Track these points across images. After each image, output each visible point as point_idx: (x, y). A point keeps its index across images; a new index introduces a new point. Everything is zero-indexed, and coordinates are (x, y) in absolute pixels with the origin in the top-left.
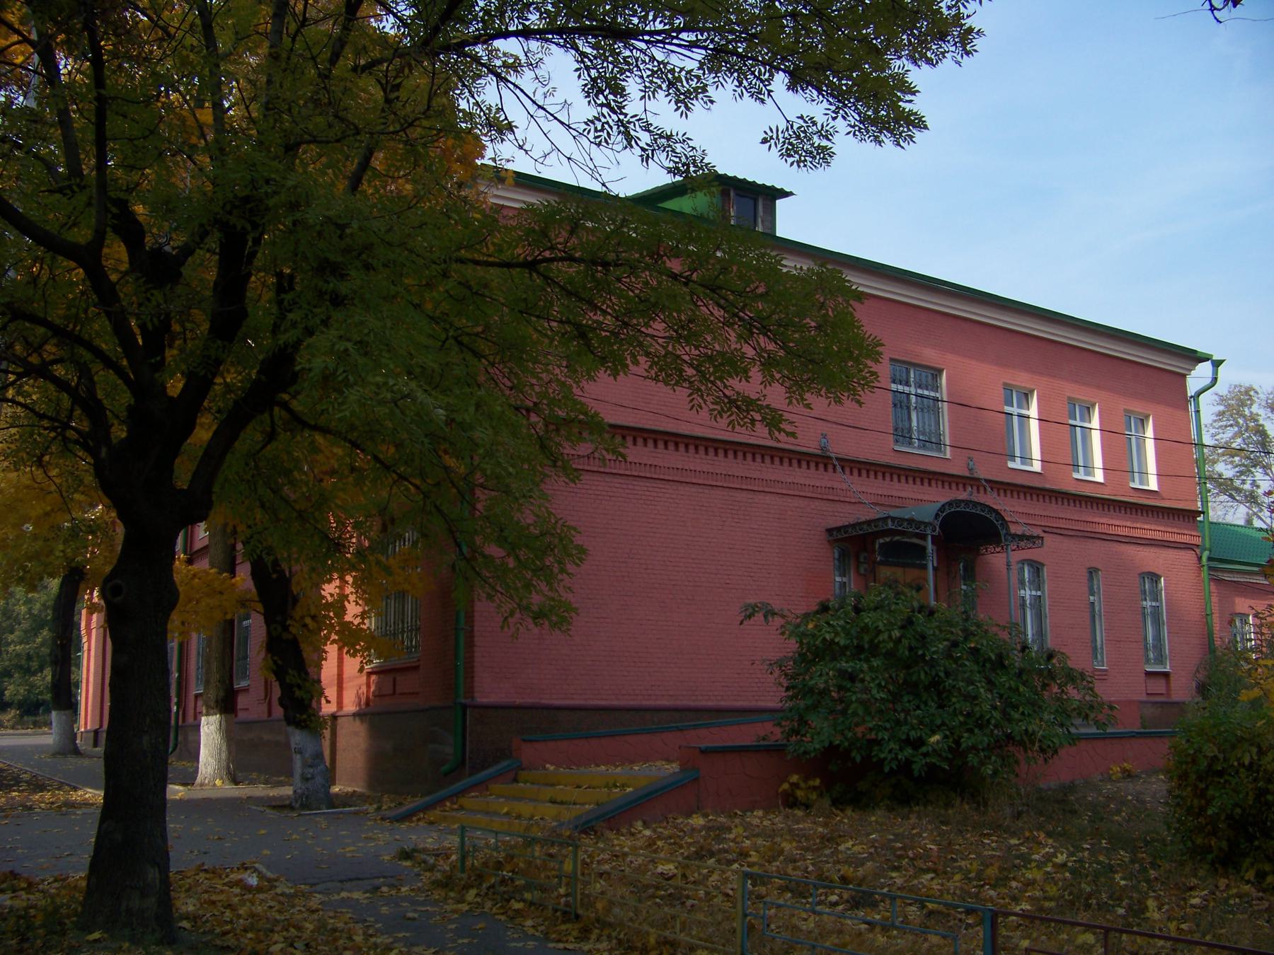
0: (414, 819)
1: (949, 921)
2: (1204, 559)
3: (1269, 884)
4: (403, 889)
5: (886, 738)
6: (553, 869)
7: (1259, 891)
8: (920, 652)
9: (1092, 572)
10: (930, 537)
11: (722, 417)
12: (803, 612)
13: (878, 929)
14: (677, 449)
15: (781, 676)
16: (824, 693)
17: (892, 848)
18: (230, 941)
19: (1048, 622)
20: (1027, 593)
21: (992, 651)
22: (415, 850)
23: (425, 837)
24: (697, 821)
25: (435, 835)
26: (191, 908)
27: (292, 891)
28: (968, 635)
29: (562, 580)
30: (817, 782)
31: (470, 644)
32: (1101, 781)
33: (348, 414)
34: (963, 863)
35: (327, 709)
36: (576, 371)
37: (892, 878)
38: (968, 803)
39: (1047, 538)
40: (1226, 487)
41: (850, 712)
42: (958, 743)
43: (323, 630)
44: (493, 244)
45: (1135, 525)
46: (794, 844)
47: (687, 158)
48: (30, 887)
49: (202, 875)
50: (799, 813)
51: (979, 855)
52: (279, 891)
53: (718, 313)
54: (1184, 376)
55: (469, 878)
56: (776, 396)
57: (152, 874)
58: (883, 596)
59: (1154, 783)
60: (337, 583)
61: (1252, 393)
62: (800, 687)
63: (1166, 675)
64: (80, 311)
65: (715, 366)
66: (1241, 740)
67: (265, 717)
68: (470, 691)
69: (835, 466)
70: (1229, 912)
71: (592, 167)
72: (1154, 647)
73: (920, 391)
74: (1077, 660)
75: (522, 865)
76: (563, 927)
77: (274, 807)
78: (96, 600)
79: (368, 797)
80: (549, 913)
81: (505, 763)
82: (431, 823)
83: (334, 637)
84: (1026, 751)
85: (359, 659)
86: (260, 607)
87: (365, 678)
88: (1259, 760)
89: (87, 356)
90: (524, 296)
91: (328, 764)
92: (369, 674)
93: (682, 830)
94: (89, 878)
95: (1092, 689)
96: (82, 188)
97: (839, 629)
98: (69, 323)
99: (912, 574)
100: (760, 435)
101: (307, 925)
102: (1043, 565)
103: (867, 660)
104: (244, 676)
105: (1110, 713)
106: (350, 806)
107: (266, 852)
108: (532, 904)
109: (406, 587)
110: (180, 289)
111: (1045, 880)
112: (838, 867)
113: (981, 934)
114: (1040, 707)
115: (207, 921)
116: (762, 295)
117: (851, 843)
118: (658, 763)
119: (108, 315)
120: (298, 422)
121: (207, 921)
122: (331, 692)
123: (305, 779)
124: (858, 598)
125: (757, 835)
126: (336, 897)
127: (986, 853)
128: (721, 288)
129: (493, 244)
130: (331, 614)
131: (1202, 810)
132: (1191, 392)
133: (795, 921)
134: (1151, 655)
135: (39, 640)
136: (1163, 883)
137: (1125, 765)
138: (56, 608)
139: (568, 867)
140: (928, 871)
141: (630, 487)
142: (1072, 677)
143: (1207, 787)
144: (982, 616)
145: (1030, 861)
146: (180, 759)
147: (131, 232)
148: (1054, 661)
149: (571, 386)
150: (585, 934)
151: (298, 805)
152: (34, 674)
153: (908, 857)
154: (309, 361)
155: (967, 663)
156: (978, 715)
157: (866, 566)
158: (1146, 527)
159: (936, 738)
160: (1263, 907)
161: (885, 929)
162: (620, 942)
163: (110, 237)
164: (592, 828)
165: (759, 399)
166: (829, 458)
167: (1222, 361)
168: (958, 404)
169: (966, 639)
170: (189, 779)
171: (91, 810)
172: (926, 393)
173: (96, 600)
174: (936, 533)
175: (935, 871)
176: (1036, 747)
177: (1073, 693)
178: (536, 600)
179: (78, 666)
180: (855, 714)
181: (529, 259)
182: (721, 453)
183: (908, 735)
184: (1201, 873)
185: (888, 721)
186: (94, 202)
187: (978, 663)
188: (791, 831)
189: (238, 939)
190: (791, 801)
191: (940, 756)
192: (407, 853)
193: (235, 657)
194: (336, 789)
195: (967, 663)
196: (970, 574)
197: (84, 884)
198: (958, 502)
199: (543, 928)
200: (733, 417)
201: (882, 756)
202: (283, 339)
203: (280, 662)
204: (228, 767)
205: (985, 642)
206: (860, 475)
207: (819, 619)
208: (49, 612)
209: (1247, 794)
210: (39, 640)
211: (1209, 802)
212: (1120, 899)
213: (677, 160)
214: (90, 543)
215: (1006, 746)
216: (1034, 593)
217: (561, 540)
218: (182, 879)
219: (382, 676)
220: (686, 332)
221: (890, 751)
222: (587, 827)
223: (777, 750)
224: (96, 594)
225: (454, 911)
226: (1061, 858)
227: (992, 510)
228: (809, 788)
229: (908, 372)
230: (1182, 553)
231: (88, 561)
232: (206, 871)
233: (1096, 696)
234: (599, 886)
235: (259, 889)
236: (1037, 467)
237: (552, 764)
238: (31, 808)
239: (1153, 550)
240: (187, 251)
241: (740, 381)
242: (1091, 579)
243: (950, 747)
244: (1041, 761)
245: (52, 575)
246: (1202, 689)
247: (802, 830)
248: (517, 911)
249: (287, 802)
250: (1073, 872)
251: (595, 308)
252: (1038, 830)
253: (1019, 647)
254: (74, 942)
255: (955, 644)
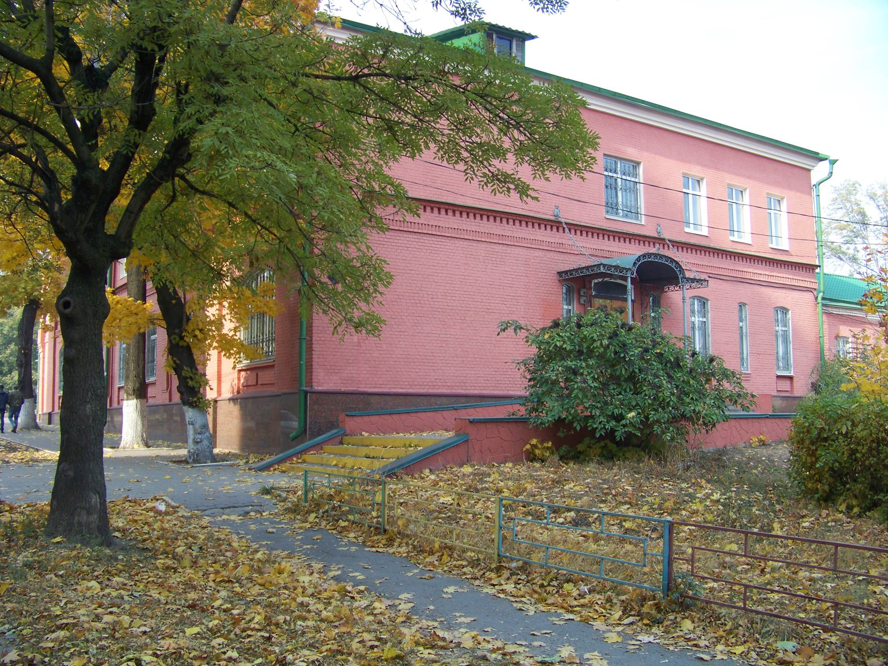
0: (272, 469)
1: (639, 536)
2: (819, 299)
3: (855, 513)
4: (264, 514)
5: (598, 414)
6: (368, 500)
7: (848, 518)
8: (622, 355)
9: (742, 305)
10: (629, 279)
11: (487, 186)
12: (542, 327)
13: (591, 540)
14: (454, 215)
15: (525, 371)
16: (555, 383)
17: (601, 488)
18: (149, 545)
19: (710, 340)
20: (697, 319)
21: (672, 355)
22: (272, 488)
23: (277, 480)
24: (467, 469)
25: (286, 479)
26: (121, 525)
27: (189, 514)
28: (655, 344)
29: (375, 297)
30: (550, 444)
31: (310, 349)
32: (744, 447)
33: (228, 176)
34: (649, 499)
35: (210, 395)
36: (385, 155)
37: (600, 508)
38: (653, 459)
39: (711, 281)
40: (838, 254)
41: (573, 396)
42: (647, 418)
43: (207, 340)
44: (328, 63)
45: (772, 274)
46: (534, 485)
47: (465, 4)
48: (12, 509)
49: (128, 504)
50: (537, 465)
51: (660, 493)
52: (180, 514)
53: (487, 114)
54: (809, 170)
55: (310, 506)
56: (525, 173)
57: (95, 499)
58: (597, 316)
59: (781, 449)
60: (217, 307)
61: (857, 185)
62: (539, 378)
63: (791, 378)
64: (38, 108)
65: (483, 151)
66: (841, 417)
67: (167, 402)
68: (310, 382)
69: (564, 229)
70: (828, 531)
71: (398, 11)
72: (783, 358)
73: (624, 177)
74: (730, 364)
75: (346, 497)
76: (376, 538)
77: (174, 462)
78: (48, 322)
79: (239, 455)
80: (366, 528)
81: (334, 431)
82: (284, 472)
83: (215, 344)
84: (693, 425)
85: (232, 360)
86: (164, 323)
87: (236, 375)
88: (852, 430)
89: (42, 140)
90: (350, 100)
91: (211, 432)
92: (240, 371)
93: (457, 476)
94: (51, 504)
95: (739, 383)
96: (36, 18)
97: (566, 339)
98: (30, 116)
99: (617, 304)
100: (511, 203)
101: (200, 536)
102: (708, 300)
103: (585, 360)
104: (153, 374)
105: (752, 399)
106: (227, 461)
107: (170, 490)
108: (354, 522)
109: (265, 309)
110: (107, 95)
111: (705, 511)
112: (564, 500)
113: (661, 544)
114: (704, 395)
115: (132, 532)
116: (516, 101)
117: (573, 484)
118: (440, 432)
119: (58, 109)
120: (192, 188)
121: (132, 532)
122: (213, 383)
123: (196, 442)
124: (580, 318)
125: (508, 479)
126: (219, 519)
127: (665, 492)
128: (487, 95)
129: (328, 63)
130: (214, 328)
131: (813, 464)
132: (814, 182)
133: (535, 534)
134: (781, 365)
135: (8, 352)
136: (784, 513)
137: (761, 437)
138: (20, 328)
139: (379, 498)
140: (625, 503)
141: (421, 241)
142: (726, 375)
143: (816, 449)
144: (665, 332)
145: (695, 498)
146: (108, 432)
147: (73, 55)
148: (714, 363)
149: (381, 165)
150: (390, 542)
151: (191, 461)
152: (5, 375)
153: (612, 494)
154: (201, 141)
155: (654, 363)
156: (661, 399)
157: (585, 298)
158: (779, 275)
159: (633, 414)
160: (850, 528)
161: (596, 539)
162: (414, 547)
163: (58, 57)
164: (394, 474)
165: (513, 174)
166: (561, 223)
167: (836, 161)
168: (651, 185)
169: (654, 346)
170: (115, 446)
171: (50, 463)
172: (628, 178)
173: (48, 322)
174: (634, 276)
175: (630, 504)
176: (701, 422)
177: (726, 384)
178: (356, 315)
179: (36, 370)
180: (576, 397)
181: (354, 74)
182: (485, 217)
183: (613, 412)
184: (810, 507)
185: (599, 402)
186: (45, 29)
187: (662, 364)
188: (531, 476)
189: (154, 544)
190: (532, 457)
191: (634, 426)
192: (267, 490)
193: (146, 361)
194: (216, 451)
195: (654, 363)
196: (657, 303)
197: (48, 508)
198: (650, 255)
199: (362, 538)
200: (495, 186)
201: (595, 426)
202: (182, 126)
203: (178, 362)
204: (142, 436)
205: (667, 350)
206: (581, 235)
207: (552, 332)
208: (16, 333)
209: (843, 452)
210: (8, 352)
211: (817, 459)
212: (755, 522)
213: (457, 5)
214: (43, 282)
215: (680, 421)
216: (701, 319)
217: (375, 269)
218: (114, 506)
219: (248, 372)
220: (461, 126)
221: (600, 423)
222: (391, 473)
223: (523, 421)
224: (48, 318)
225: (301, 528)
226: (716, 496)
227: (672, 260)
228: (544, 448)
229: (616, 164)
230: (805, 294)
231: (42, 295)
232: (130, 501)
233: (742, 388)
234: (399, 511)
235: (167, 513)
236: (705, 231)
237: (366, 432)
238: (8, 462)
239: (784, 291)
240: (112, 68)
241: (500, 162)
242: (741, 310)
243: (641, 421)
244: (704, 431)
245: (17, 305)
246: (815, 387)
247: (539, 476)
248: (344, 527)
249: (184, 459)
250: (724, 505)
251: (400, 109)
252: (701, 478)
253: (690, 353)
254: (43, 543)
255: (646, 350)
